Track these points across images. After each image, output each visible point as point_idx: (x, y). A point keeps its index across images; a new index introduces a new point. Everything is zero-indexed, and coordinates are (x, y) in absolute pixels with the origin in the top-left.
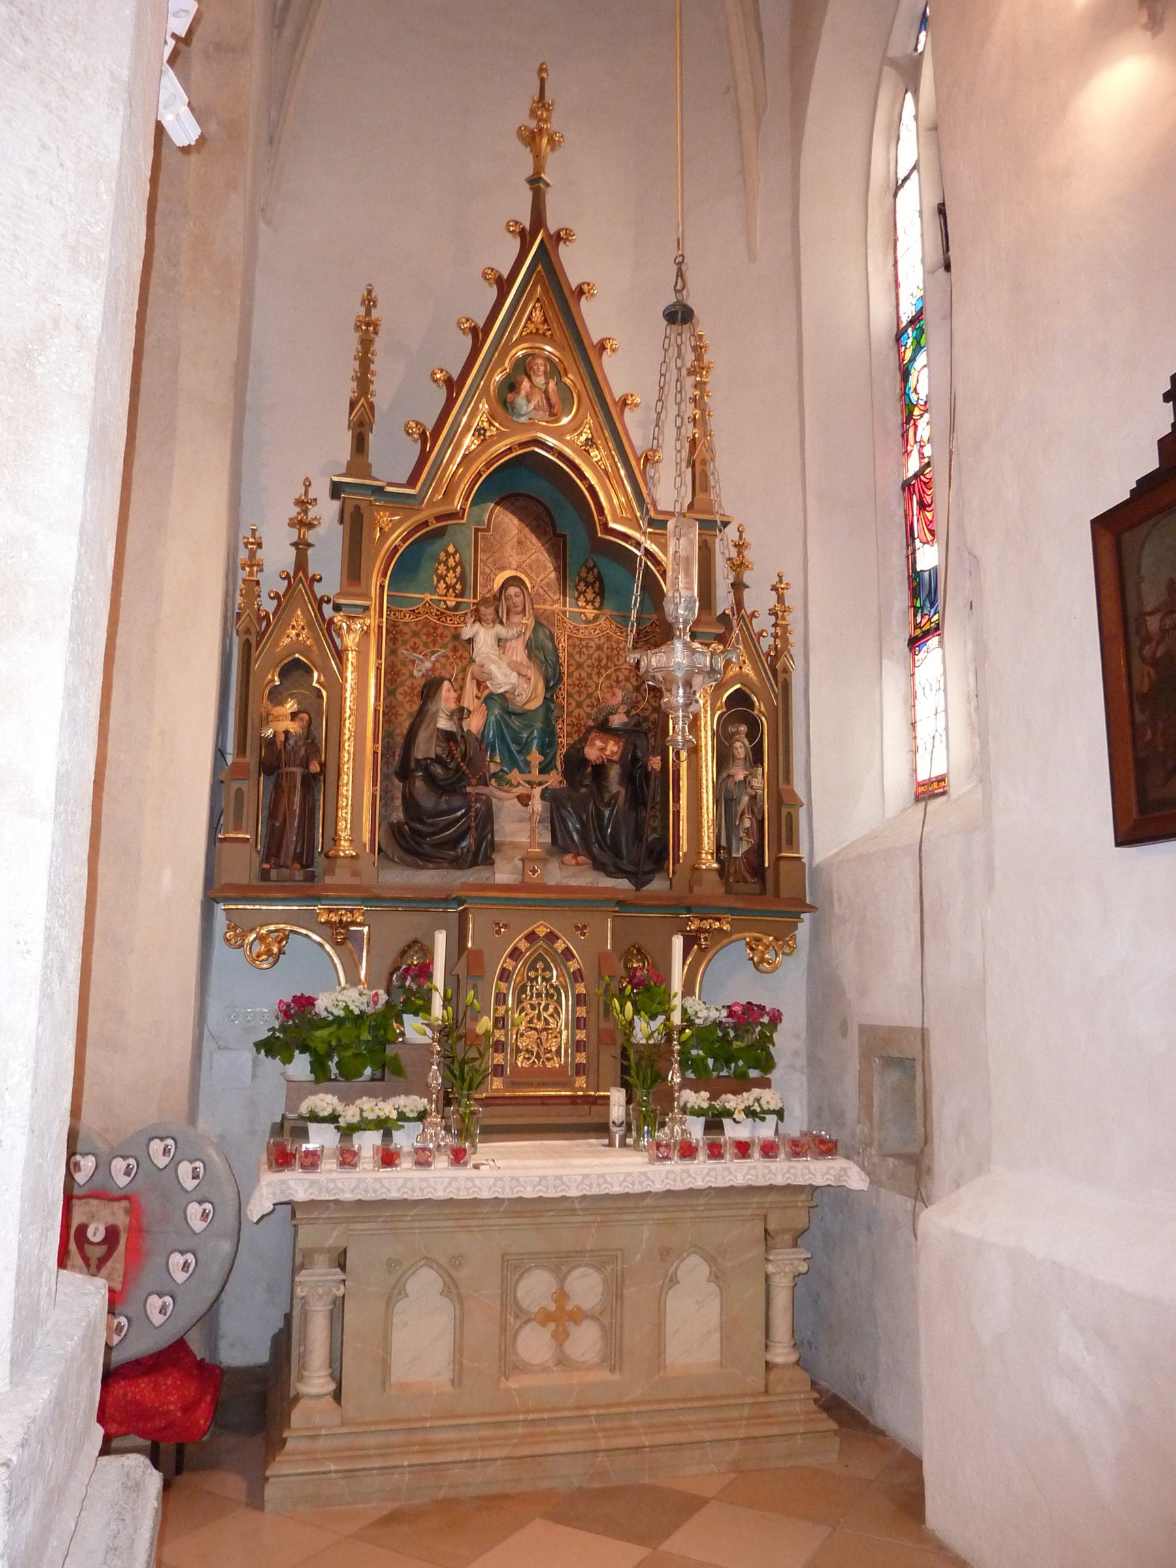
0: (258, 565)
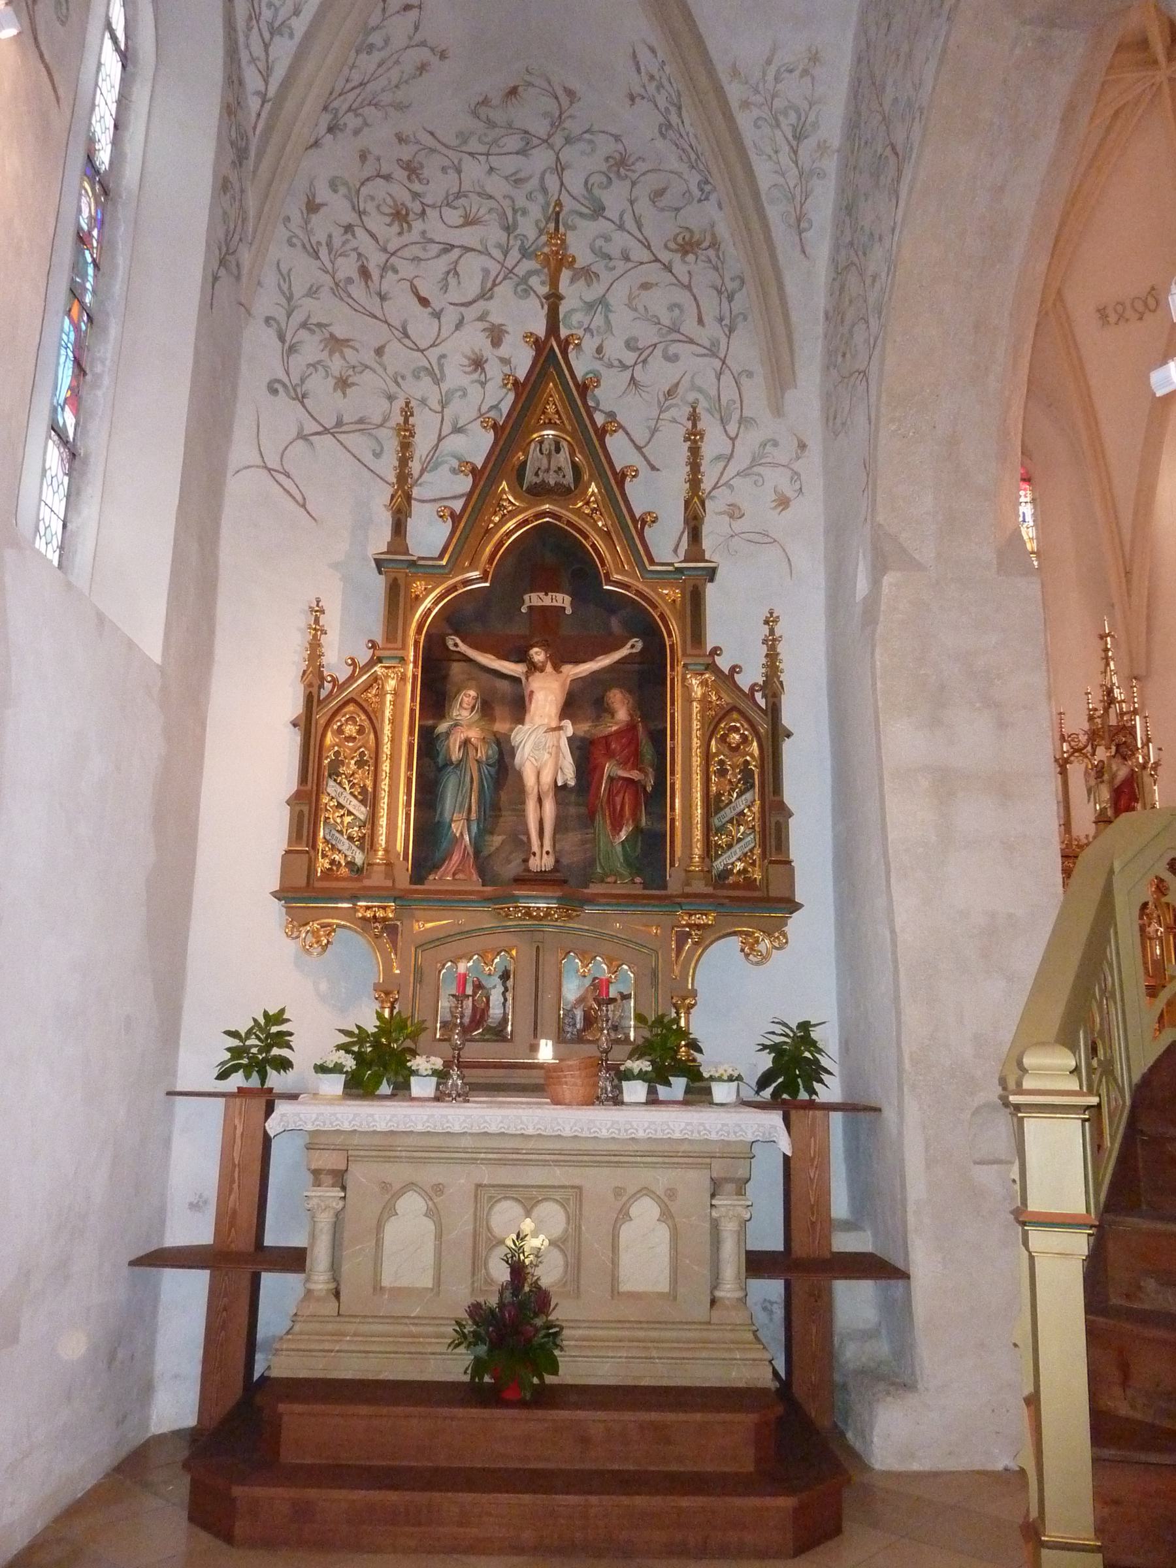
0: (322, 631)
